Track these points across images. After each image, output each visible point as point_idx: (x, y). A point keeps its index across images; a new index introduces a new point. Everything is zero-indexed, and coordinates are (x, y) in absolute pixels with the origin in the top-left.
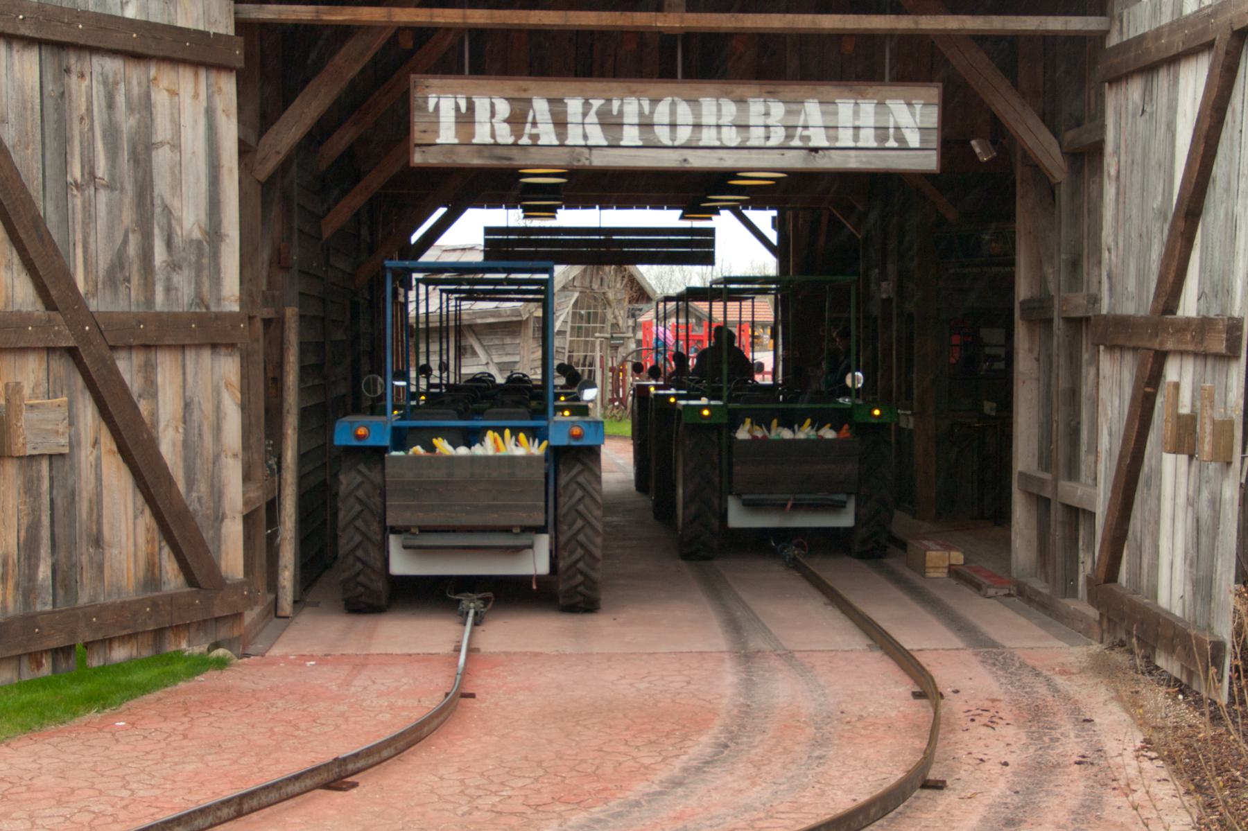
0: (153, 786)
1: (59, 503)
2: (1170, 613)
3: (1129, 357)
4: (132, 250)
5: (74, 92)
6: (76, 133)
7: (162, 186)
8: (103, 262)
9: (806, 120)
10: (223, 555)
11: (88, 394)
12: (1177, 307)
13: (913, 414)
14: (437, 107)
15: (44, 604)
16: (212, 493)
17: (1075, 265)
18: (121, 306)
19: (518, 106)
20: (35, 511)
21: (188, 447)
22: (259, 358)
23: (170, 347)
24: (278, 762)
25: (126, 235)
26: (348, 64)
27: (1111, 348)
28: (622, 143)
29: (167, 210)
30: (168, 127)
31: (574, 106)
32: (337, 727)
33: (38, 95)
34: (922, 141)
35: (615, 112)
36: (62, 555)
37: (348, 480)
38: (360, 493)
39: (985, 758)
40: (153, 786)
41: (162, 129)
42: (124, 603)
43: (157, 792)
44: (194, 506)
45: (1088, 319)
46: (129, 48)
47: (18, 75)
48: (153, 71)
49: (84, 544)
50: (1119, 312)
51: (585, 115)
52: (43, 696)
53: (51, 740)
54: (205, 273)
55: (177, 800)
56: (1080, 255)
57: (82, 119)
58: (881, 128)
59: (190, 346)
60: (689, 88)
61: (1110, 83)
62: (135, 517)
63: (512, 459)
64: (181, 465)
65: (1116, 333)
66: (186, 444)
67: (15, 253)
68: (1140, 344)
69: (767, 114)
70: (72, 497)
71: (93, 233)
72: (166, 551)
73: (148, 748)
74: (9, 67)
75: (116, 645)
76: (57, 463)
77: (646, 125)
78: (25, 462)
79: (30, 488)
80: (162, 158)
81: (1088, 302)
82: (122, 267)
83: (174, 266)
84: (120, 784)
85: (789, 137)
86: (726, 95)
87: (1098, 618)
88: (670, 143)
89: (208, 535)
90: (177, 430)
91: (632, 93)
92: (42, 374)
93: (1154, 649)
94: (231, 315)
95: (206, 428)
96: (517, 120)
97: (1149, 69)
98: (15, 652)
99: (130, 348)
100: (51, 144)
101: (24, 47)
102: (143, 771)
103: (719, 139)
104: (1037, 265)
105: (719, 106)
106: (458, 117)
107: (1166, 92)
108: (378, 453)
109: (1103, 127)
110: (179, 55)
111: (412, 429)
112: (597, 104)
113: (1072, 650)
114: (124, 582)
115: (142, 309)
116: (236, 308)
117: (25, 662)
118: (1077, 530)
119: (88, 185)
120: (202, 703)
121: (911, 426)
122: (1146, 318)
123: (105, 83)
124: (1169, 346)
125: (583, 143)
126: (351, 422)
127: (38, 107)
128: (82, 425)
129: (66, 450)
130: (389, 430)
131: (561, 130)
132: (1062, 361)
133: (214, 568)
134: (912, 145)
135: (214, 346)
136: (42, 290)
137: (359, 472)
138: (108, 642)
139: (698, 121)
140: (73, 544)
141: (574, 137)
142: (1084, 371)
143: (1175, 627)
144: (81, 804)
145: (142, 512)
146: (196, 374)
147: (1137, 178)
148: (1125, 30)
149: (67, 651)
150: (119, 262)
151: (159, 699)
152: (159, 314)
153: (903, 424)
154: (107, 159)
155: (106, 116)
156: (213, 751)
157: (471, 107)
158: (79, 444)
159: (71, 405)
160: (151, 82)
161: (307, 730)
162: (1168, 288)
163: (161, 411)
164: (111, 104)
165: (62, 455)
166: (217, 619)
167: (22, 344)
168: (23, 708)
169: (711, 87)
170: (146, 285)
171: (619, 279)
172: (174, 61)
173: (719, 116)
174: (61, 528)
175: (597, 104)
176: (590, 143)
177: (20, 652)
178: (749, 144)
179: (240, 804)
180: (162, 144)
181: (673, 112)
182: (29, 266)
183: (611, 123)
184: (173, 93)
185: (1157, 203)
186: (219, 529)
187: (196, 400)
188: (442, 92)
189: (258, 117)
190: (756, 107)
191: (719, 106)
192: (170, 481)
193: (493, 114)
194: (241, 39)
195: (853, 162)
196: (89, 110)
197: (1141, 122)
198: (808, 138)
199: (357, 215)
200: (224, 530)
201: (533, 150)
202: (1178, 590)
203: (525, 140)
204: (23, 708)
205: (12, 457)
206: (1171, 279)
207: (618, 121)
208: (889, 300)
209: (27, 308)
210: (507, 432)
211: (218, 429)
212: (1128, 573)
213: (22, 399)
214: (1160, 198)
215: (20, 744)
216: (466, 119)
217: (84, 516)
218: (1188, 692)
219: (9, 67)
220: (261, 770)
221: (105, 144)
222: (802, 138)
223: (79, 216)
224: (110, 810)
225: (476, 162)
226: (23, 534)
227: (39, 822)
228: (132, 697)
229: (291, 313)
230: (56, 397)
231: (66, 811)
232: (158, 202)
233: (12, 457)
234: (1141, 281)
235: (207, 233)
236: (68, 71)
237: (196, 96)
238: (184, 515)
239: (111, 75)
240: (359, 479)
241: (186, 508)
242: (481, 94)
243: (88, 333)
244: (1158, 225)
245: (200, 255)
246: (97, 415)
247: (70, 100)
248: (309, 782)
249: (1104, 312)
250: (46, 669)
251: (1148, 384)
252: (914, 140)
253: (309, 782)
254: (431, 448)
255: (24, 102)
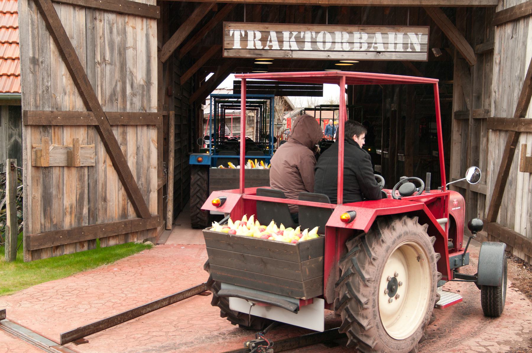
0: (133, 293)
1: (91, 184)
2: (520, 234)
3: (503, 134)
4: (119, 88)
5: (98, 27)
6: (99, 43)
7: (130, 64)
8: (108, 93)
9: (376, 40)
10: (150, 206)
11: (102, 143)
12: (525, 115)
13: (404, 155)
14: (233, 34)
15: (85, 223)
16: (146, 182)
17: (479, 98)
18: (114, 110)
19: (264, 34)
20: (82, 188)
21: (138, 164)
22: (162, 130)
23: (132, 125)
24: (179, 285)
25: (116, 83)
26: (196, 17)
27: (495, 131)
28: (304, 49)
29: (131, 73)
30: (132, 41)
31: (286, 35)
32: (198, 272)
33: (85, 28)
34: (421, 49)
35: (302, 37)
36: (92, 204)
37: (194, 178)
38: (199, 183)
39: (450, 289)
40: (133, 293)
41: (130, 42)
42: (114, 223)
43: (136, 295)
44: (140, 187)
45: (484, 120)
46: (118, 10)
47: (77, 20)
48: (127, 19)
49: (100, 200)
50: (499, 116)
51: (290, 38)
52: (84, 258)
53: (90, 275)
54: (145, 97)
55: (143, 298)
56: (481, 94)
57: (101, 37)
58: (407, 43)
59: (139, 125)
60: (330, 28)
61: (498, 26)
62: (119, 191)
63: (258, 171)
64: (135, 171)
65: (498, 125)
66: (137, 163)
67: (76, 89)
68: (509, 129)
69: (361, 38)
70: (96, 182)
71: (104, 82)
72: (130, 203)
73: (129, 278)
74: (75, 17)
75: (111, 239)
76: (91, 169)
77: (314, 42)
78: (79, 169)
79: (81, 179)
80: (130, 53)
81: (485, 112)
82: (115, 95)
83: (134, 95)
84: (120, 292)
85: (369, 47)
86: (345, 30)
87: (487, 236)
88: (323, 49)
89: (145, 198)
90: (134, 158)
91: (309, 29)
92: (86, 136)
93: (512, 248)
94: (154, 114)
95: (145, 157)
96: (264, 40)
97: (516, 20)
98: (75, 241)
99: (117, 126)
100: (89, 47)
101: (80, 9)
102: (128, 287)
103: (342, 48)
104: (463, 96)
105: (342, 35)
106: (242, 39)
107: (522, 30)
108: (206, 168)
109: (493, 44)
110: (137, 13)
111: (218, 158)
112: (295, 34)
113: (476, 248)
114: (114, 215)
115: (122, 111)
116: (156, 111)
117: (78, 245)
118: (477, 201)
119: (103, 63)
120: (145, 262)
121: (404, 160)
122: (512, 119)
123: (109, 24)
124: (522, 130)
125: (289, 49)
126: (196, 156)
127: (85, 33)
128: (100, 155)
129: (94, 165)
130: (210, 159)
131: (281, 44)
132: (472, 135)
133: (146, 209)
134: (417, 51)
135: (148, 126)
136: (86, 103)
137: (199, 175)
138: (108, 238)
139: (334, 41)
140: (96, 201)
141: (286, 46)
142: (481, 139)
143: (523, 240)
144: (107, 299)
145: (121, 189)
146: (141, 136)
147: (508, 64)
148: (505, 4)
149: (93, 241)
150: (114, 93)
151: (128, 260)
152: (129, 113)
153: (400, 159)
154: (110, 53)
155: (109, 37)
156: (153, 280)
157: (246, 35)
158: (99, 162)
159: (96, 147)
160: (126, 23)
161: (187, 272)
162: (522, 107)
163: (128, 150)
164: (111, 32)
165: (92, 166)
166: (148, 230)
167: (78, 124)
168: (78, 262)
169: (339, 27)
170: (123, 102)
171: (280, 101)
172: (135, 15)
173: (342, 39)
174: (92, 195)
175: (295, 34)
176: (292, 49)
177: (77, 241)
178: (353, 50)
179: (170, 300)
180: (130, 47)
181: (324, 37)
182: (81, 94)
183: (300, 41)
184: (134, 28)
185: (517, 73)
186: (149, 196)
187: (141, 146)
188: (235, 28)
189: (164, 36)
190: (357, 35)
191: (342, 35)
192: (132, 177)
193: (255, 37)
194: (159, 7)
195: (394, 57)
196: (103, 34)
197: (511, 42)
198: (377, 48)
199: (194, 75)
200: (150, 196)
201: (270, 51)
202: (524, 225)
203: (267, 48)
204: (78, 262)
205: (75, 167)
206: (523, 104)
207: (303, 40)
208: (395, 111)
209: (80, 110)
210: (256, 160)
211: (149, 157)
212: (501, 217)
213: (79, 145)
214: (519, 72)
215: (79, 276)
216: (244, 39)
217: (100, 190)
218: (527, 265)
219: (75, 17)
220: (173, 287)
221: (109, 47)
222: (374, 47)
223: (99, 75)
224: (119, 302)
225: (248, 56)
226: (78, 196)
227: (93, 305)
228: (118, 259)
229: (172, 113)
230: (90, 144)
231: (102, 302)
232: (128, 70)
233: (75, 167)
234: (509, 104)
235: (146, 82)
236: (95, 19)
237: (142, 29)
238: (137, 190)
239: (111, 21)
240: (199, 177)
241: (137, 187)
242: (250, 30)
243: (102, 120)
244: (518, 82)
245: (143, 91)
246: (105, 151)
247: (96, 30)
248: (194, 292)
249: (492, 116)
250: (86, 248)
251: (512, 145)
252: (418, 48)
253: (194, 292)
254: (227, 166)
255: (80, 31)
